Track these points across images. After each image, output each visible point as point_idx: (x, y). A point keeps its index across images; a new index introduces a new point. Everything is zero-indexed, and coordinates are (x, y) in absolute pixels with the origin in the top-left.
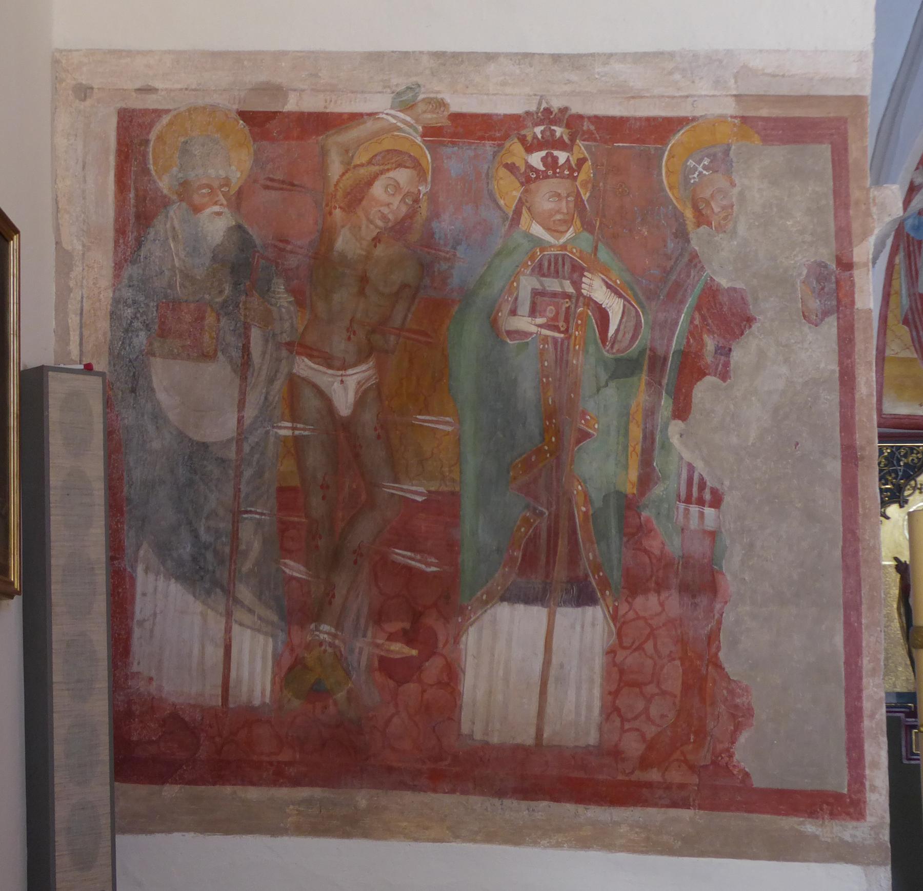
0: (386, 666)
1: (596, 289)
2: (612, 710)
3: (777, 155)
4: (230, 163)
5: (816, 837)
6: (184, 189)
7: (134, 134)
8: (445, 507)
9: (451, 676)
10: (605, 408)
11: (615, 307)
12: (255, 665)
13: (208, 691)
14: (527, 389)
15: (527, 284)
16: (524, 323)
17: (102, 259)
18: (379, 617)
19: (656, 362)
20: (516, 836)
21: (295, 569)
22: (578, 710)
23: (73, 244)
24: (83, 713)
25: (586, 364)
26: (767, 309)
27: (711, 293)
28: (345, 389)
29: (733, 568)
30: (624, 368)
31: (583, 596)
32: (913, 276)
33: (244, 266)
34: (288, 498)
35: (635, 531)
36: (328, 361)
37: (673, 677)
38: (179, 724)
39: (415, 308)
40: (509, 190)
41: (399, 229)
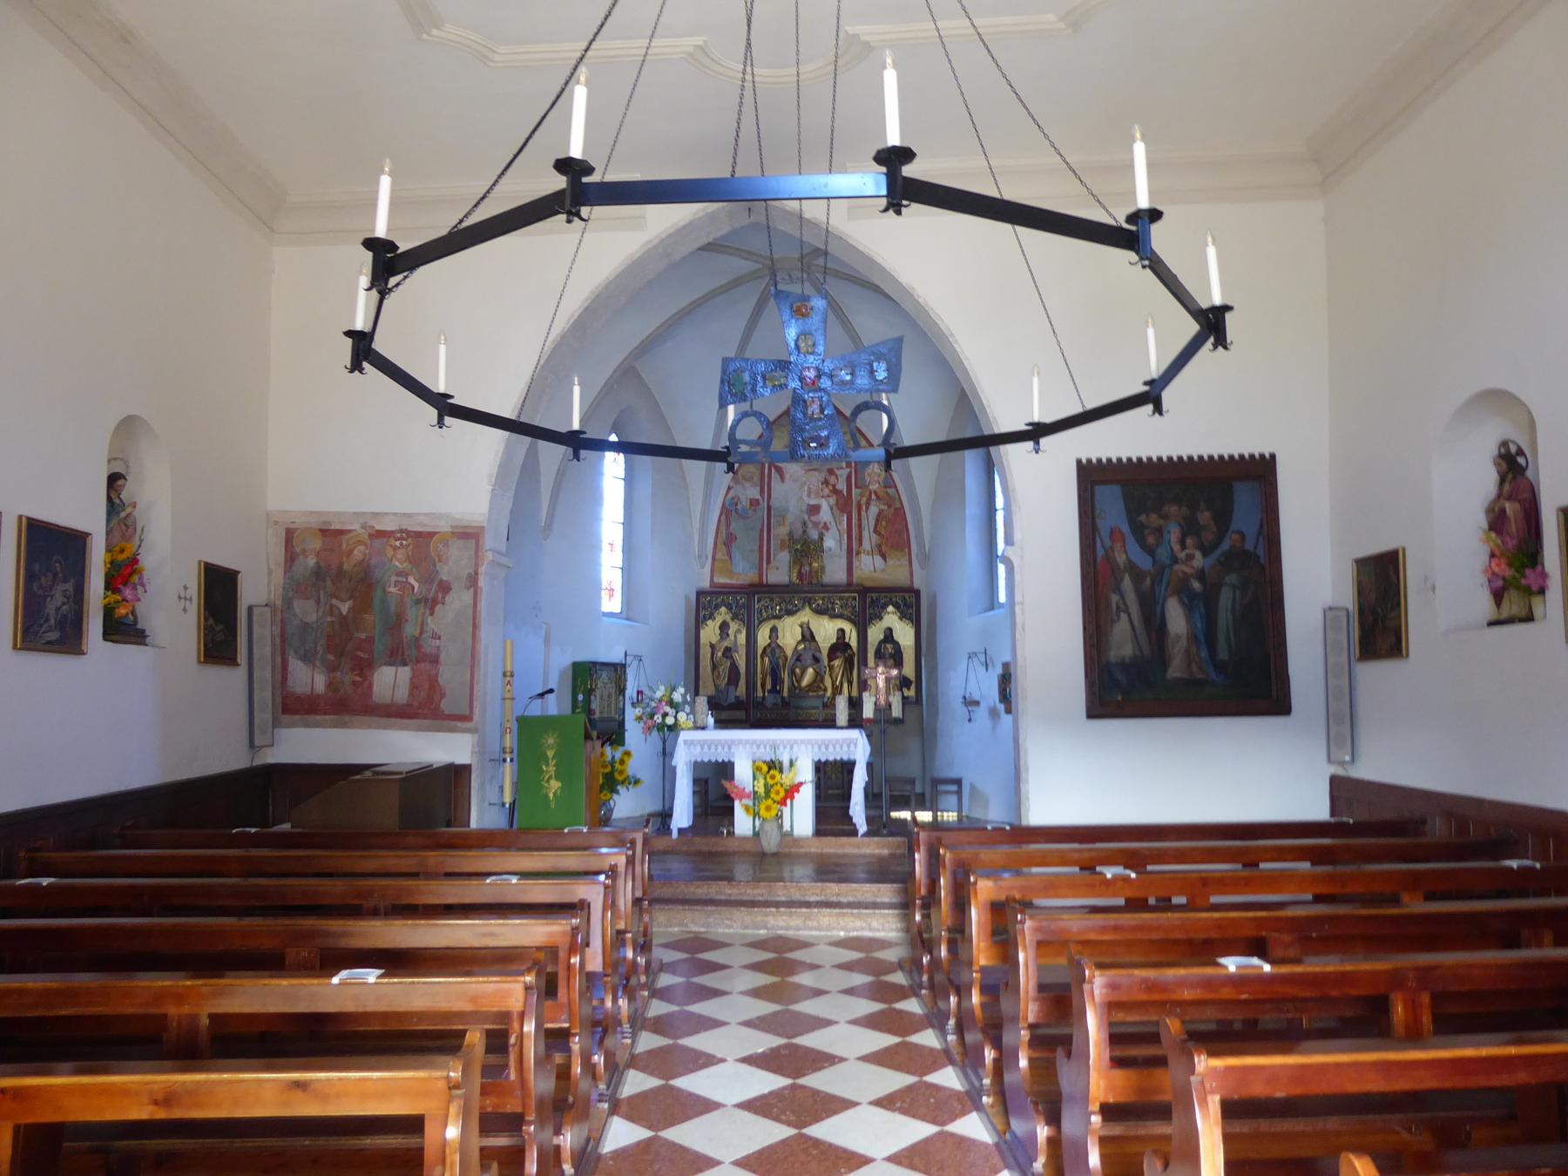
0: (354, 683)
1: (412, 580)
2: (411, 694)
3: (461, 543)
4: (316, 544)
5: (870, 766)
6: (304, 551)
7: (290, 535)
8: (370, 640)
9: (371, 686)
10: (412, 613)
11: (416, 585)
12: (320, 683)
13: (308, 690)
14: (393, 608)
15: (394, 578)
16: (392, 589)
17: (281, 571)
18: (352, 670)
19: (426, 600)
20: (385, 728)
21: (331, 657)
22: (402, 695)
23: (272, 566)
24: (265, 695)
25: (407, 600)
26: (455, 586)
27: (441, 581)
28: (344, 608)
29: (443, 656)
30: (418, 602)
31: (405, 664)
32: (728, 525)
33: (319, 574)
34: (330, 638)
35: (419, 647)
36: (341, 600)
37: (426, 686)
38: (299, 699)
39: (363, 585)
40: (390, 552)
41: (360, 563)
